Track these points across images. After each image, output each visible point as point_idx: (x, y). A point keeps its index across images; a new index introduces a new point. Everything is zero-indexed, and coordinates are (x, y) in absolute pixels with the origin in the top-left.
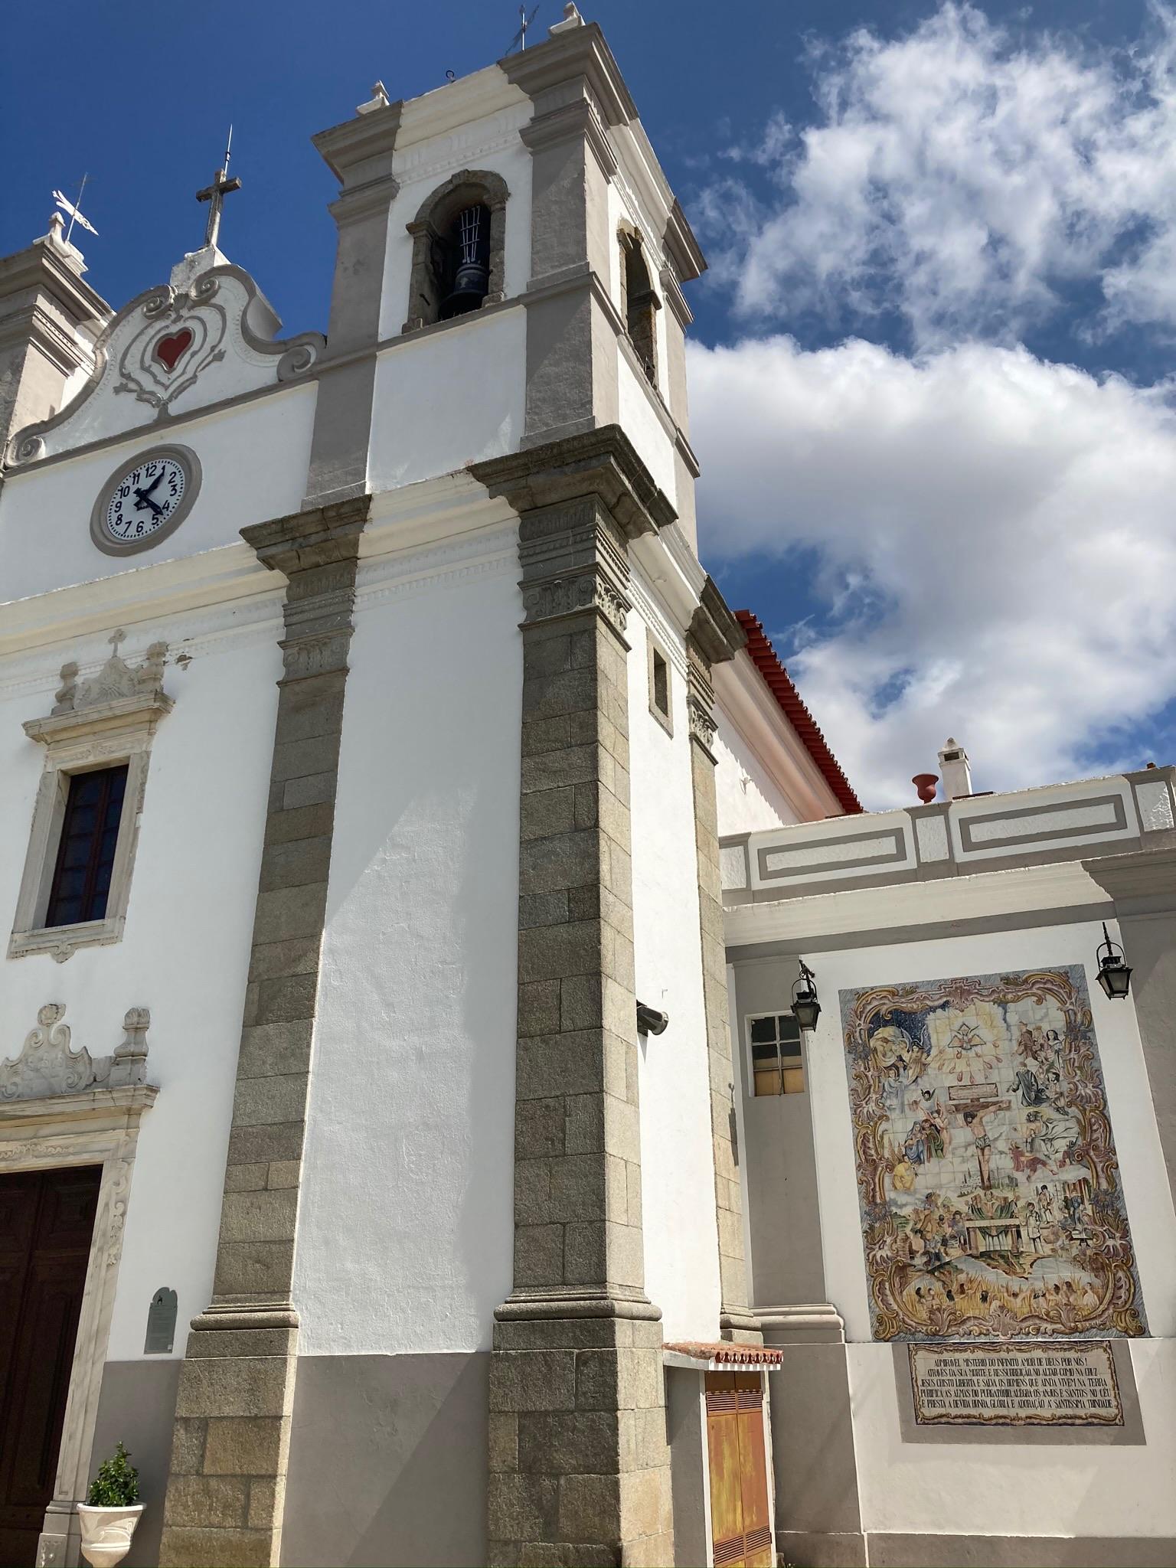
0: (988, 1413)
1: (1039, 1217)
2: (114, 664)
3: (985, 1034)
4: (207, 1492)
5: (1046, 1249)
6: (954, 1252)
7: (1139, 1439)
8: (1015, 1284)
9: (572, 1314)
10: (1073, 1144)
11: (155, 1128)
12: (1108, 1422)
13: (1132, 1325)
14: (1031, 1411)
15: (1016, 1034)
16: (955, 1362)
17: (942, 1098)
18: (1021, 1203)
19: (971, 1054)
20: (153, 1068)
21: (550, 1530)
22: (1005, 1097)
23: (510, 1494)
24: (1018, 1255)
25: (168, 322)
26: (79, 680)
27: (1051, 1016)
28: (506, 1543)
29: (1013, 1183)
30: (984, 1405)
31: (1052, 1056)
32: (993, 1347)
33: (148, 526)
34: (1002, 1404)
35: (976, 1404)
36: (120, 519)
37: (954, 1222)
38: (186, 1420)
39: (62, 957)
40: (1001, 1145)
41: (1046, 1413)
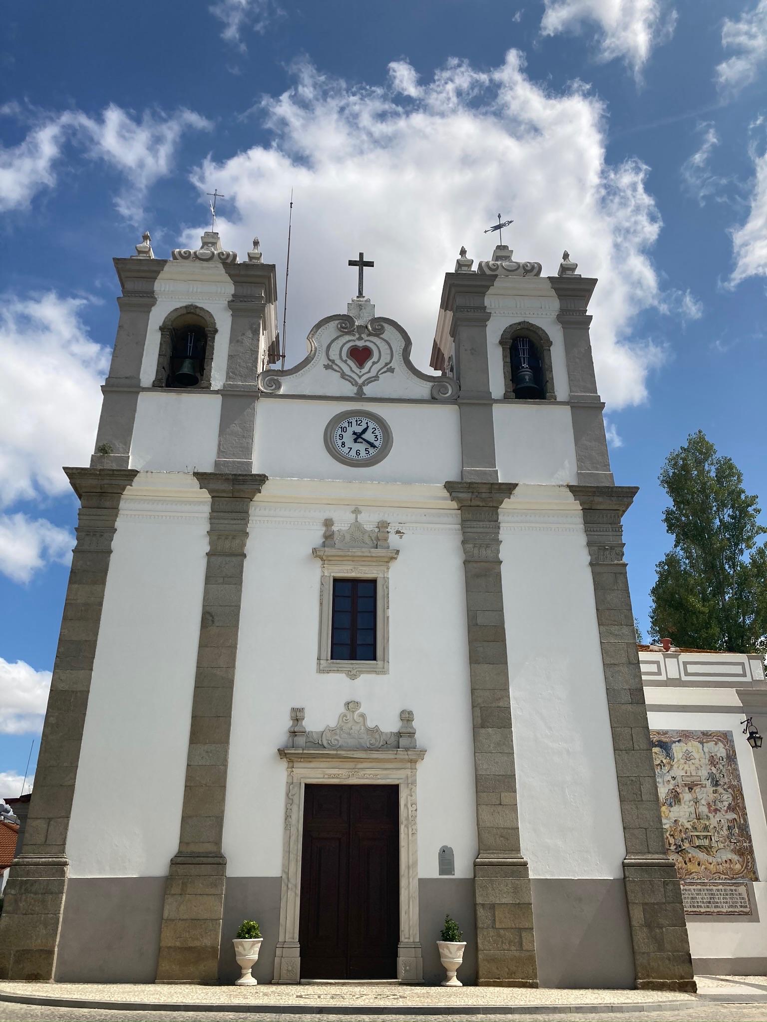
0: (703, 910)
1: (718, 833)
2: (357, 525)
3: (695, 754)
4: (499, 936)
5: (721, 846)
6: (686, 845)
7: (757, 920)
8: (710, 859)
9: (658, 865)
10: (730, 804)
11: (425, 771)
12: (746, 914)
13: (753, 877)
14: (719, 910)
15: (708, 757)
16: (690, 890)
17: (679, 780)
18: (712, 826)
19: (690, 763)
20: (420, 738)
21: (661, 948)
22: (704, 782)
23: (641, 935)
24: (711, 847)
25: (353, 338)
26: (335, 528)
27: (720, 751)
28: (644, 953)
29: (708, 818)
30: (701, 907)
31: (721, 767)
32: (704, 884)
33: (363, 453)
34: (708, 907)
35: (698, 907)
36: (343, 444)
37: (686, 833)
38: (483, 905)
39: (353, 677)
40: (703, 802)
41: (724, 910)
